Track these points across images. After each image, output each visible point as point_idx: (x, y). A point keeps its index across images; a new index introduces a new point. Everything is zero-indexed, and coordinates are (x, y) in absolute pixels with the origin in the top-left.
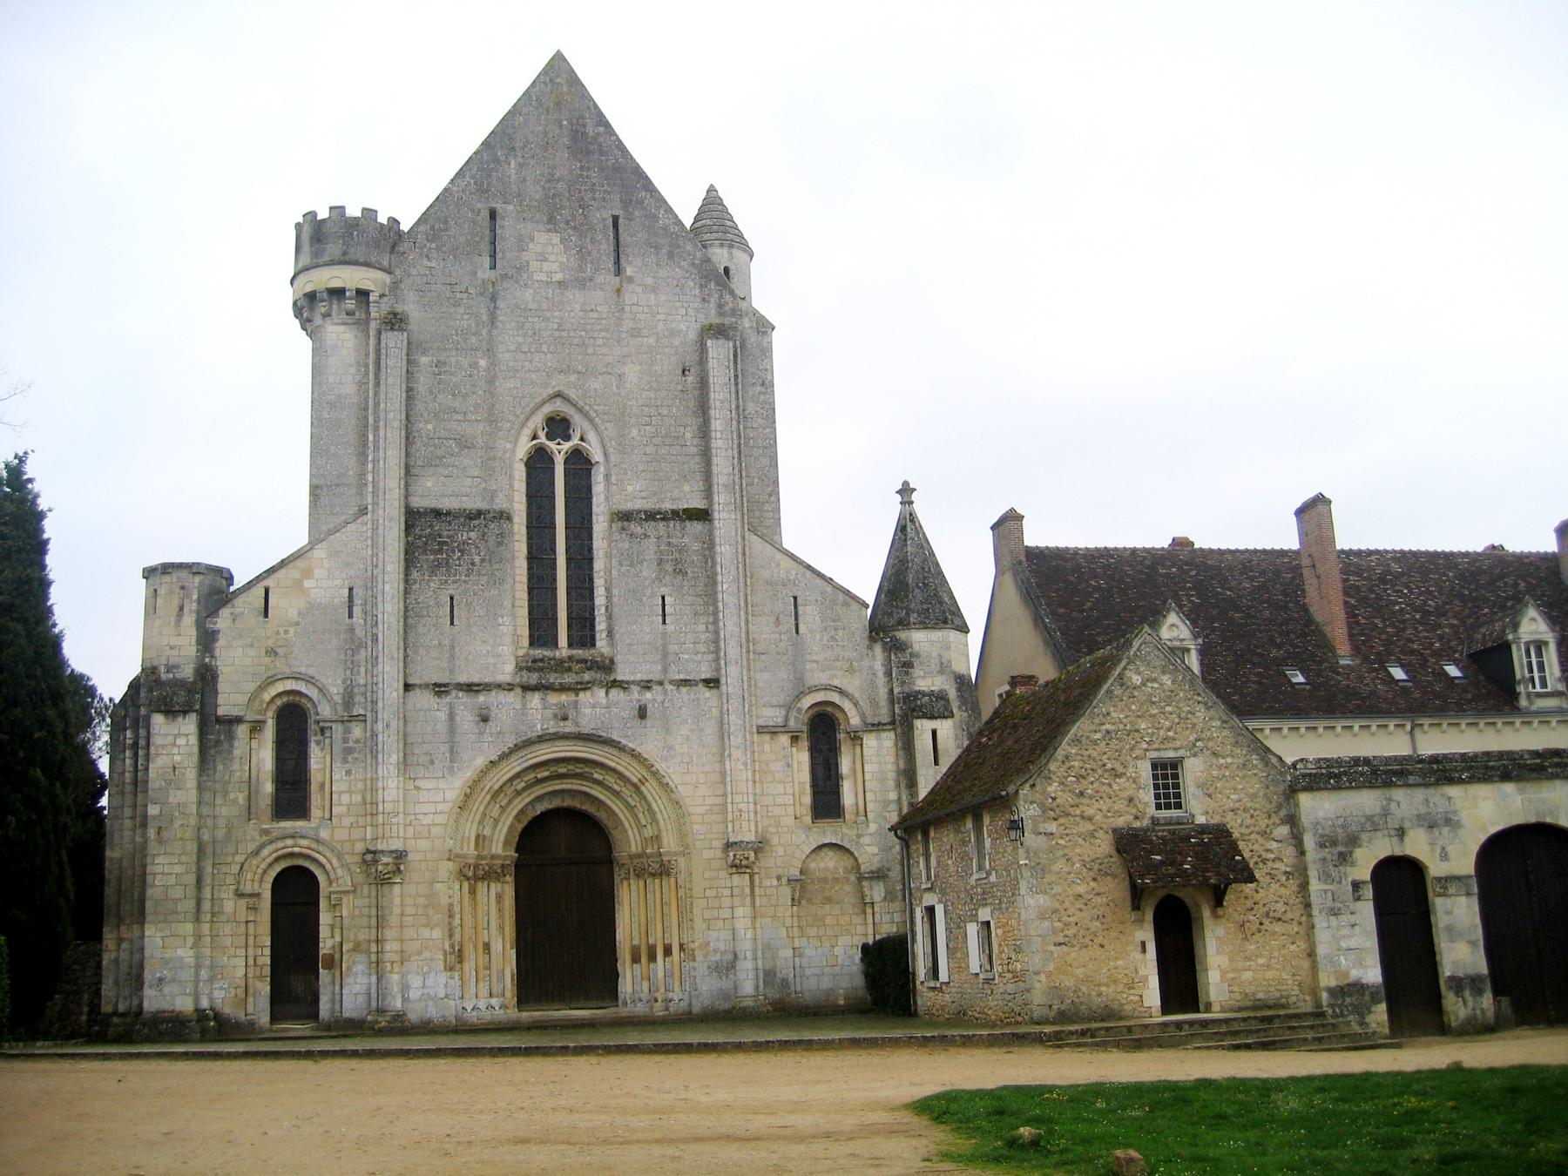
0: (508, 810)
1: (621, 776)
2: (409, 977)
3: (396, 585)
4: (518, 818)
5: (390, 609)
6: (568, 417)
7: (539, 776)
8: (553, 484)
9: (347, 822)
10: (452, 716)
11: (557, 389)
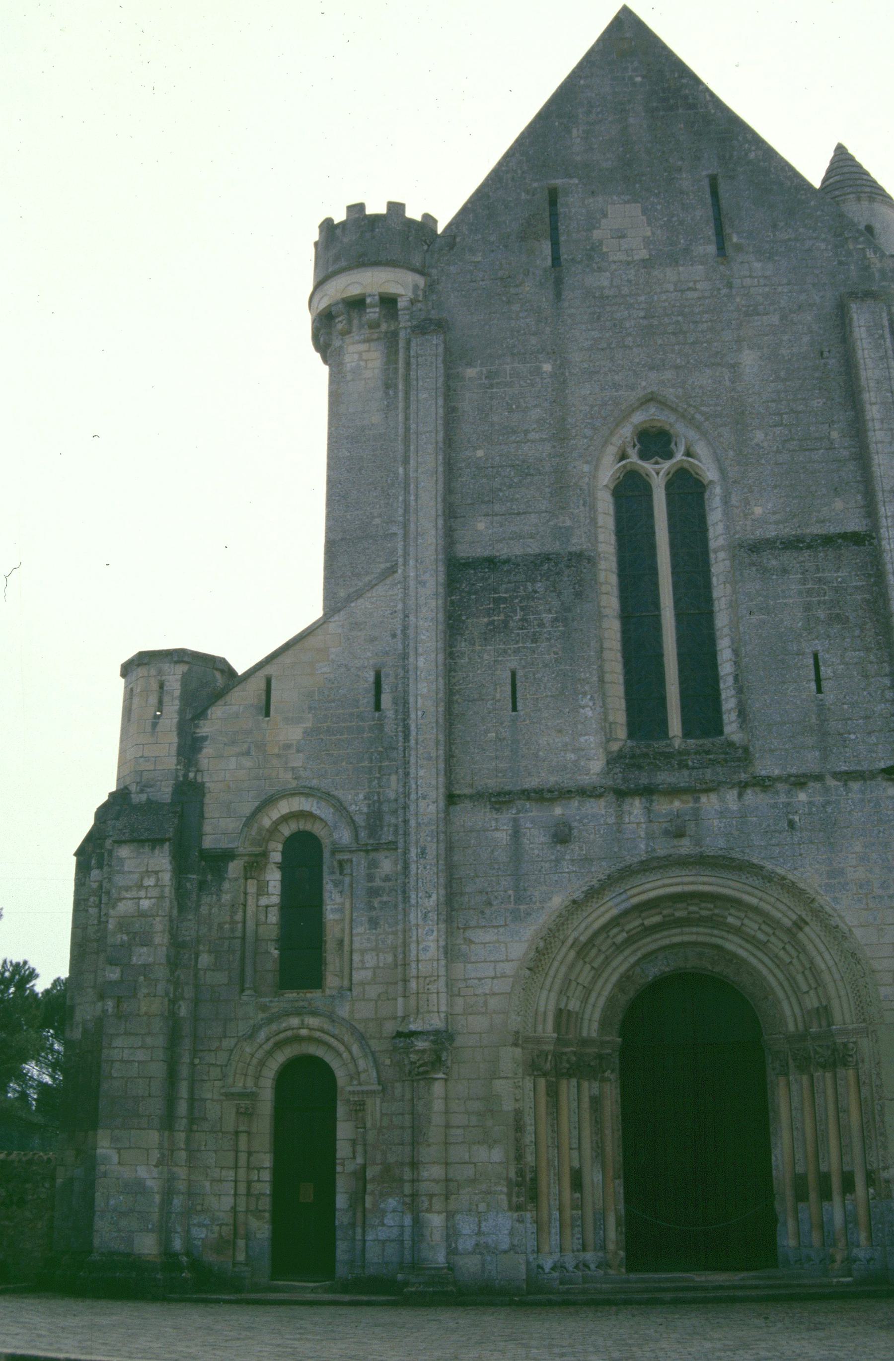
0: (605, 975)
1: (767, 919)
2: (458, 1217)
3: (433, 656)
4: (620, 985)
5: (425, 690)
6: (667, 427)
7: (647, 922)
8: (651, 515)
9: (372, 992)
10: (516, 834)
11: (649, 391)
